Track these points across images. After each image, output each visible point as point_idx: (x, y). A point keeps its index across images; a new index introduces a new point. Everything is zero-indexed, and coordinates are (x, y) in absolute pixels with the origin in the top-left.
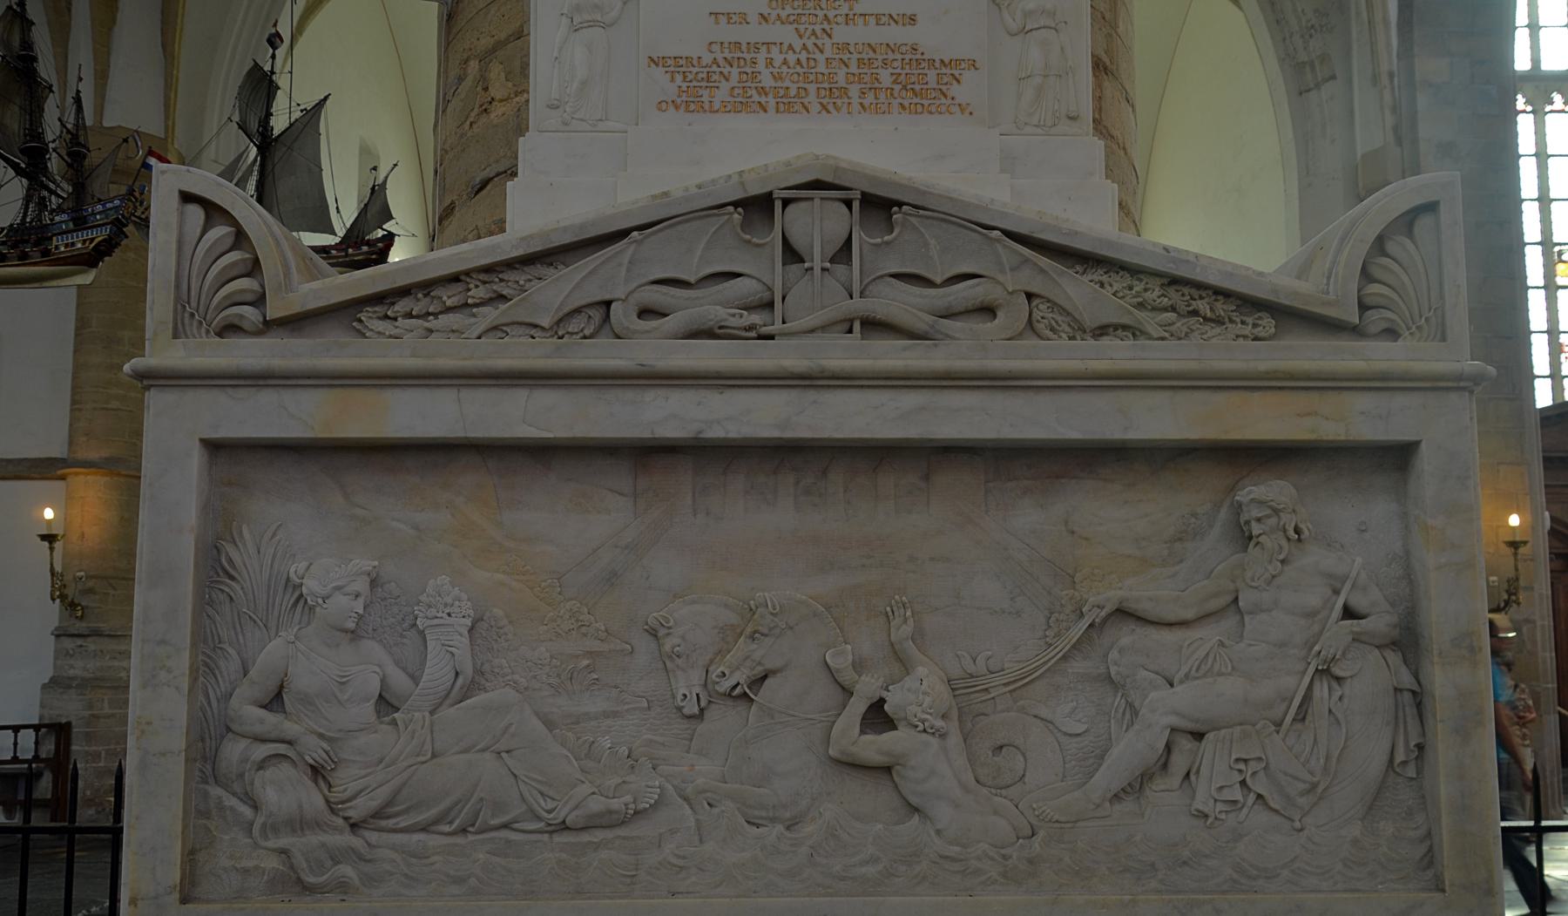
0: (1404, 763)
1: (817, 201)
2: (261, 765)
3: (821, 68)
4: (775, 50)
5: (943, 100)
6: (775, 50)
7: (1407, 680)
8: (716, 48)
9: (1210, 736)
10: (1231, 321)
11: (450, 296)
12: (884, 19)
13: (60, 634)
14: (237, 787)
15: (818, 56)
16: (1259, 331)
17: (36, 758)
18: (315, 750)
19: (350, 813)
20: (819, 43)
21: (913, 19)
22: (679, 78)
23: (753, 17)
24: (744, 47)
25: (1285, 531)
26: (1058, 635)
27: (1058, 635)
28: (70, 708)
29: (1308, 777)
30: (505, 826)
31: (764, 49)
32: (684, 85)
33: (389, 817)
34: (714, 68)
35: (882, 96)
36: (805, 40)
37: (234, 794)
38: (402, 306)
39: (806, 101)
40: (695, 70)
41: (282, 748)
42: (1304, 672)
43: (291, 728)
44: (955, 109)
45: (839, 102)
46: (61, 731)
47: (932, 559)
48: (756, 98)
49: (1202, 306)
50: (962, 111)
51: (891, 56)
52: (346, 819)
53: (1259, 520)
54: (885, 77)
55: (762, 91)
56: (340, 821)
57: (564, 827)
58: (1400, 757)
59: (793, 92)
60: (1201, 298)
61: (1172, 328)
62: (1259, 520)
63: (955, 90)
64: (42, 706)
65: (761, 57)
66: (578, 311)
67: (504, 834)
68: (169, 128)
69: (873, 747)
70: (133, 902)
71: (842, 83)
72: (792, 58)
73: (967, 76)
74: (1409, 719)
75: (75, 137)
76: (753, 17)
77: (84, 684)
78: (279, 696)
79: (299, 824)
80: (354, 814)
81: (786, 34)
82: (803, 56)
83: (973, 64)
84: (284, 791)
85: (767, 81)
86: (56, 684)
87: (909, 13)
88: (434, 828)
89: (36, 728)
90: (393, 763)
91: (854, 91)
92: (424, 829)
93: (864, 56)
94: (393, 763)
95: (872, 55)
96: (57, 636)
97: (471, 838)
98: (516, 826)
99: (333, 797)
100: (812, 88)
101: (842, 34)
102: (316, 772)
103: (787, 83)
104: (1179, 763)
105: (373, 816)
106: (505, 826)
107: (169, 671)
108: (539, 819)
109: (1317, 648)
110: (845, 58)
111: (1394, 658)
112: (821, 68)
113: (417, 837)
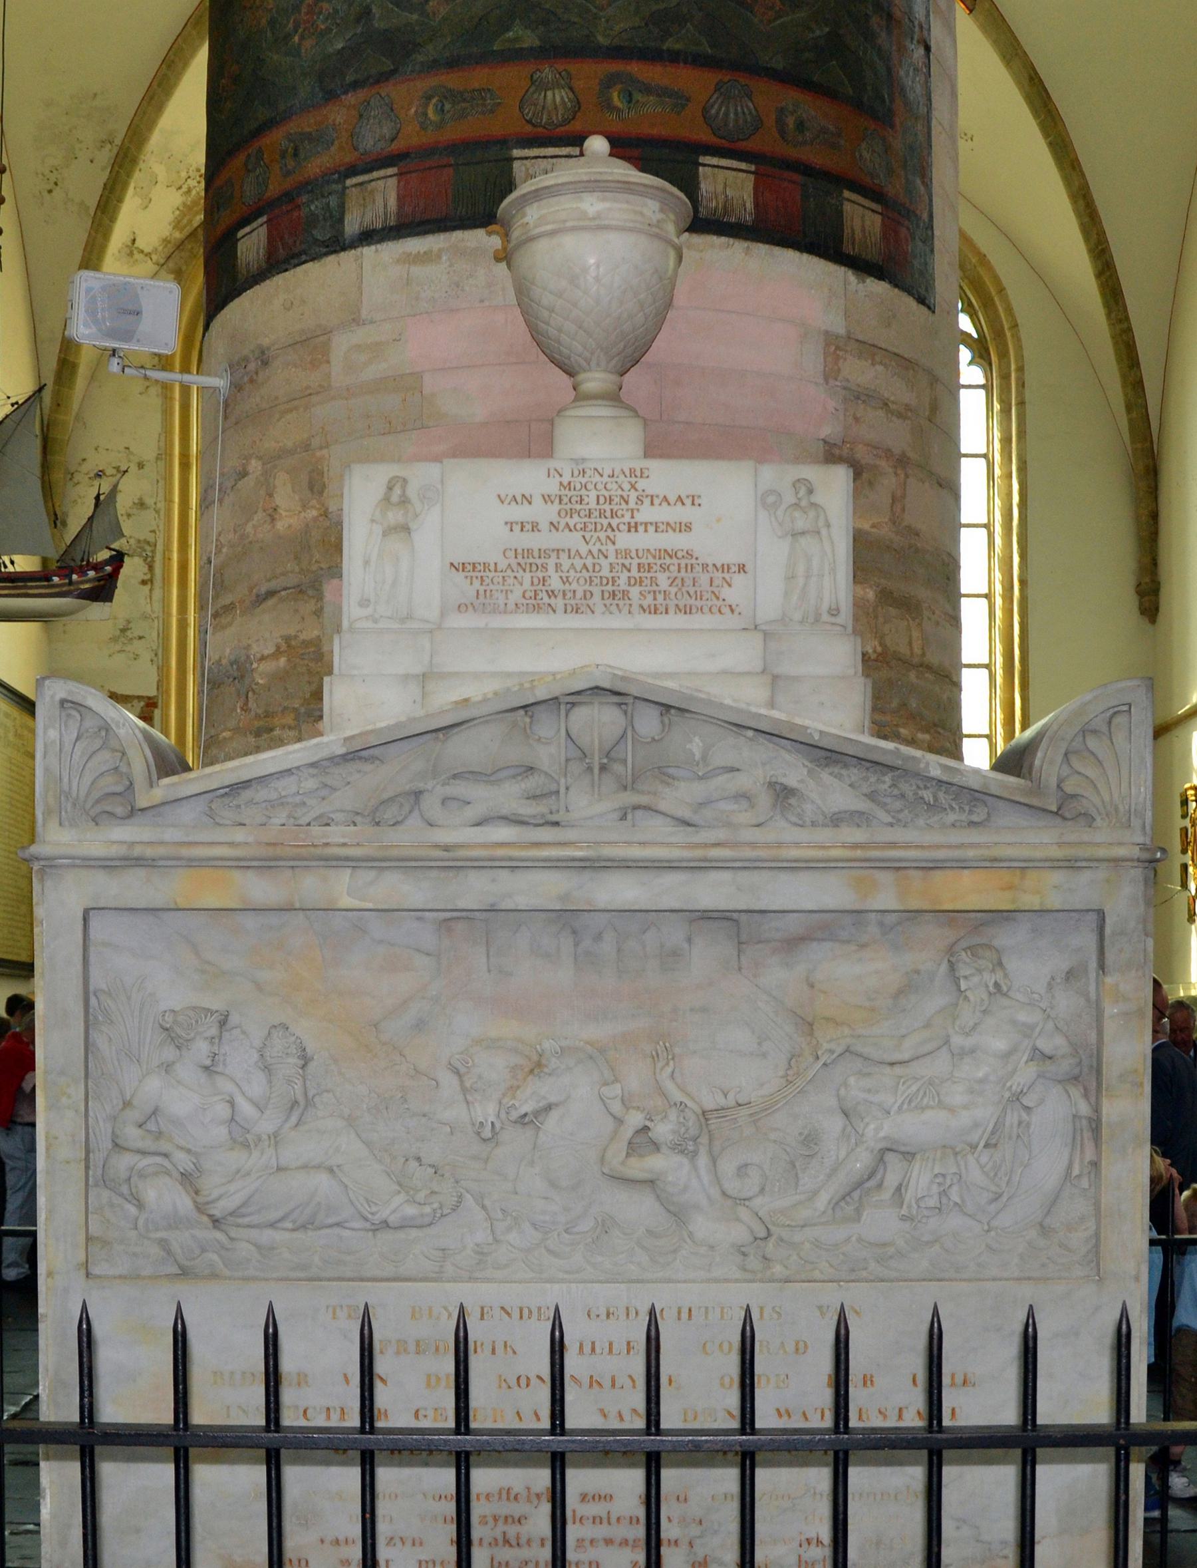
0: (1079, 1176)
1: (596, 705)
3: (605, 572)
4: (564, 556)
5: (715, 601)
6: (564, 556)
7: (1084, 1108)
8: (511, 554)
9: (918, 1157)
10: (952, 809)
12: (662, 527)
14: (125, 1189)
15: (602, 561)
16: (975, 818)
18: (183, 1161)
19: (212, 1212)
20: (603, 548)
21: (689, 527)
22: (477, 583)
23: (544, 526)
24: (536, 554)
25: (987, 986)
26: (798, 1074)
27: (798, 1074)
29: (993, 1188)
30: (338, 1224)
31: (554, 555)
32: (482, 589)
33: (244, 1216)
34: (509, 572)
35: (660, 597)
36: (590, 546)
37: (121, 1195)
39: (591, 602)
40: (491, 575)
44: (726, 610)
45: (621, 603)
47: (692, 1010)
48: (546, 600)
49: (927, 795)
50: (732, 611)
51: (668, 561)
52: (210, 1216)
53: (965, 977)
54: (663, 580)
55: (552, 594)
56: (205, 1219)
57: (385, 1224)
58: (1076, 1172)
59: (579, 594)
60: (926, 788)
61: (901, 816)
62: (965, 977)
63: (726, 592)
65: (551, 563)
66: (391, 800)
67: (337, 1230)
68: (139, 698)
69: (638, 1167)
70: (50, 1274)
71: (623, 587)
72: (578, 563)
73: (738, 579)
74: (1086, 1141)
76: (544, 526)
79: (175, 1222)
80: (217, 1213)
81: (574, 540)
82: (589, 562)
83: (742, 568)
84: (163, 1195)
85: (555, 583)
87: (684, 521)
88: (279, 1225)
90: (248, 1174)
91: (634, 592)
92: (272, 1225)
93: (643, 561)
94: (248, 1174)
95: (651, 560)
97: (310, 1233)
98: (346, 1225)
99: (200, 1199)
100: (597, 591)
101: (625, 540)
103: (574, 586)
104: (892, 1179)
105: (231, 1214)
106: (338, 1224)
107: (69, 1097)
108: (366, 1219)
109: (1008, 1084)
110: (627, 562)
111: (1076, 1092)
112: (605, 572)
113: (269, 1233)
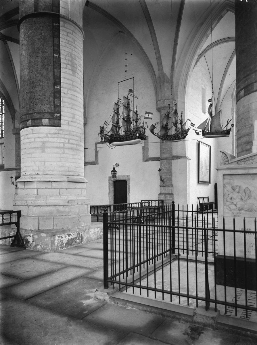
2: (230, 204)
11: (247, 159)
13: (161, 186)
17: (158, 206)
18: (235, 203)
28: (162, 197)
38: (242, 160)
41: (232, 203)
42: (203, 242)
43: (233, 201)
46: (162, 202)
64: (159, 198)
75: (181, 121)
77: (165, 194)
78: (231, 198)
79: (234, 210)
86: (160, 194)
89: (158, 201)
96: (160, 186)
102: (235, 205)
